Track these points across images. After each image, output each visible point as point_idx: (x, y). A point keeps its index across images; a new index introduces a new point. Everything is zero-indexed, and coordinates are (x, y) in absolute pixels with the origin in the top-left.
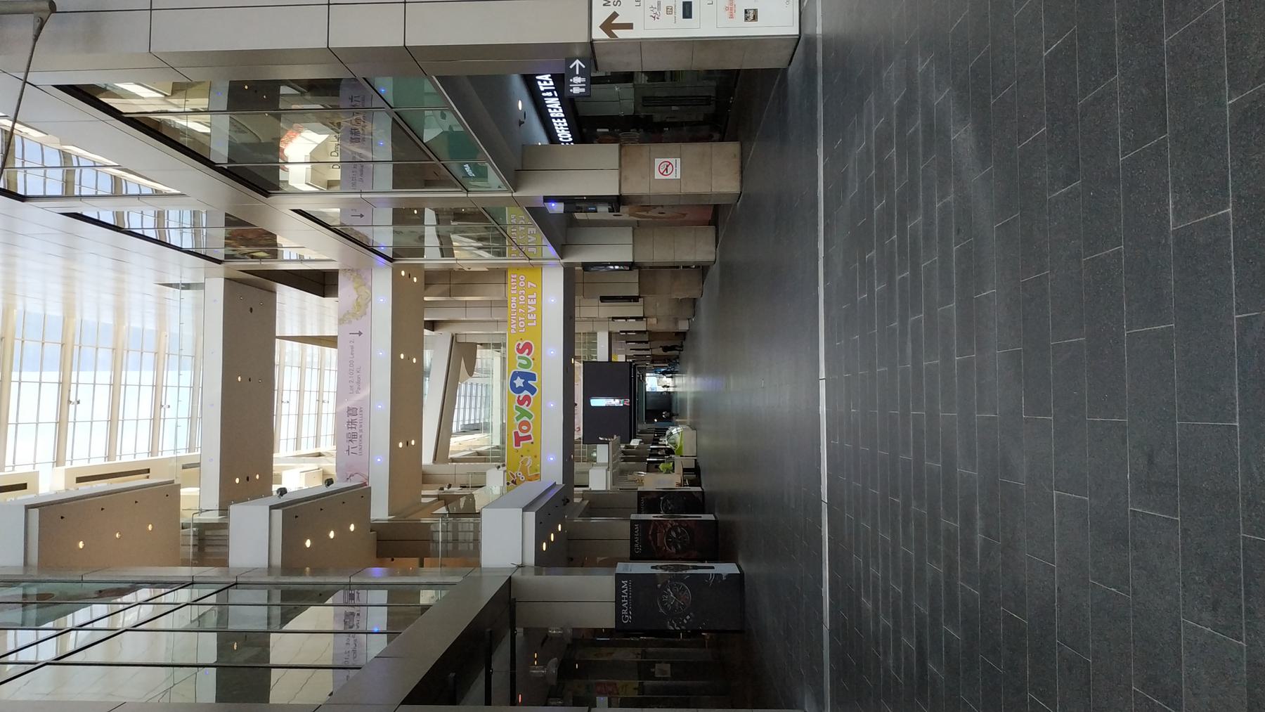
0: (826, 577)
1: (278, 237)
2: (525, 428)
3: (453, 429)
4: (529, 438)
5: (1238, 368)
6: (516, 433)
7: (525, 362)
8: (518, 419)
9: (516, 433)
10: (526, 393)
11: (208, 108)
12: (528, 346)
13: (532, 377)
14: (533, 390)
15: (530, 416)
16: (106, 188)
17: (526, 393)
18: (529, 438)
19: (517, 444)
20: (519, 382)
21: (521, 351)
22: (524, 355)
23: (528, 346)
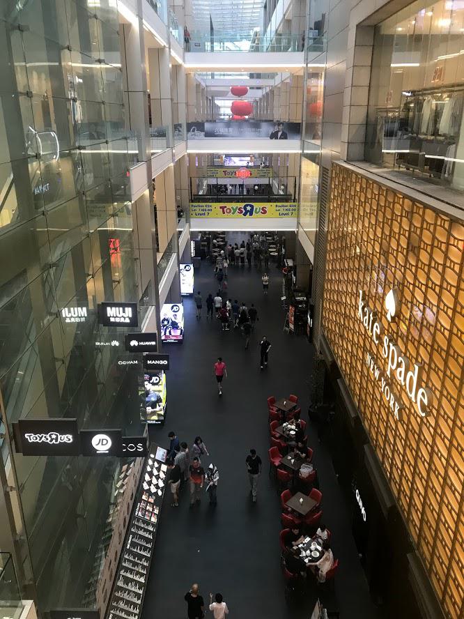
8: (232, 208)
13: (251, 214)
14: (245, 215)
18: (224, 213)
19: (221, 208)
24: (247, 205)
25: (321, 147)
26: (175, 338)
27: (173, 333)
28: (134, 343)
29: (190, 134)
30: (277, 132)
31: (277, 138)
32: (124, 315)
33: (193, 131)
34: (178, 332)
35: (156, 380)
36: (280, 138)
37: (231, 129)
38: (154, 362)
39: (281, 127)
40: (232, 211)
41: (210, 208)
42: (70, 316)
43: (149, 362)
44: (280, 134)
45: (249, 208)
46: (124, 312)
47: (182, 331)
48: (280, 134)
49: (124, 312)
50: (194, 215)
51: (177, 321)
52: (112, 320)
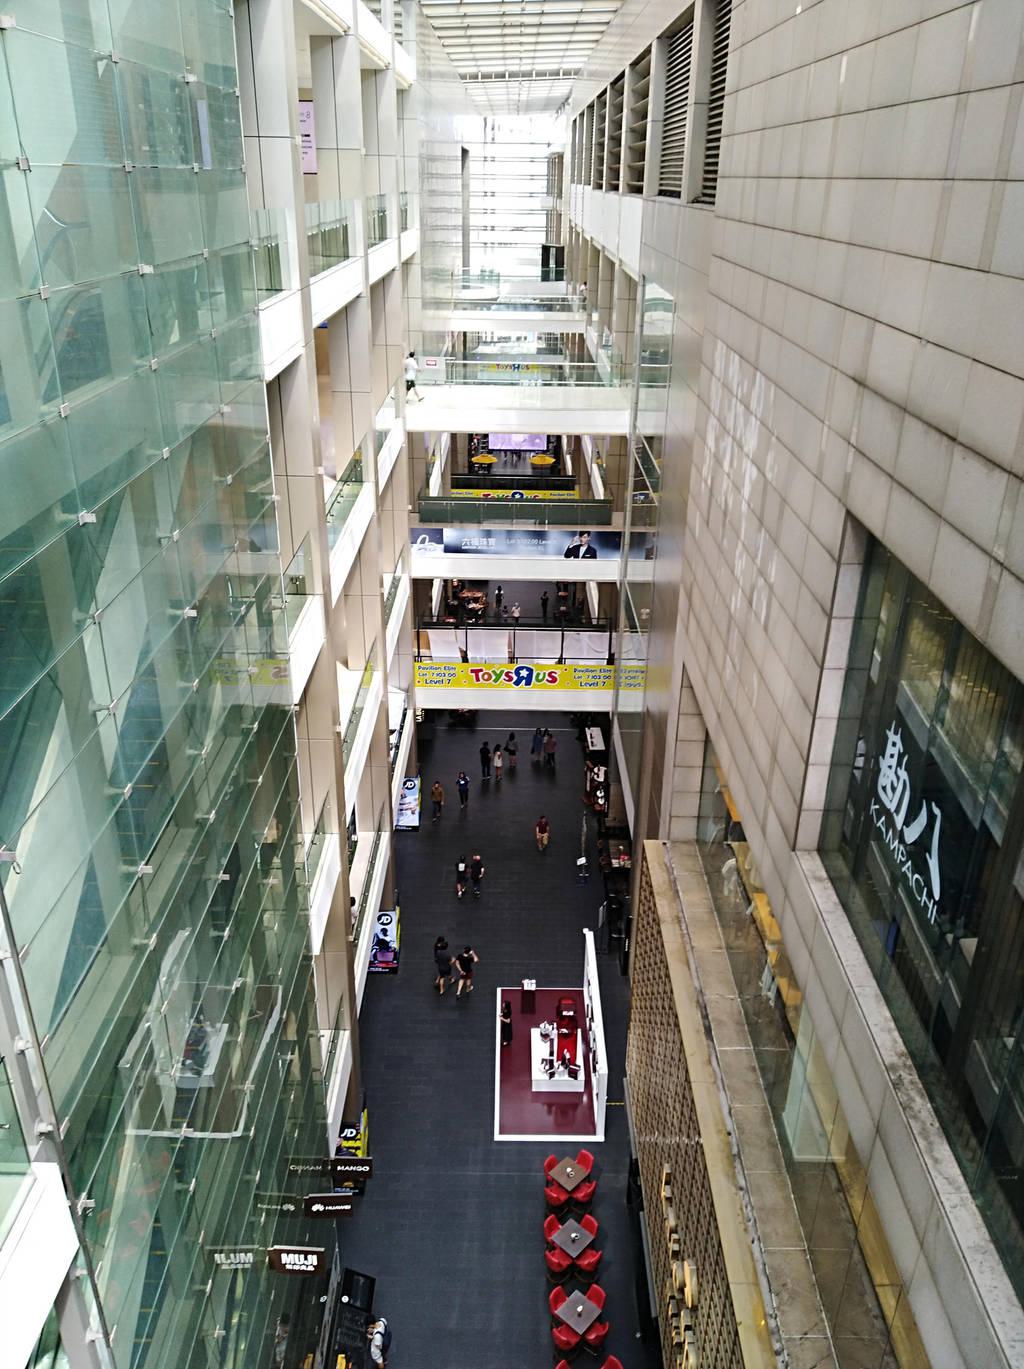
0: (594, 609)
1: (271, 572)
2: (486, 677)
3: (268, 945)
4: (478, 680)
5: (246, 1231)
6: (481, 670)
7: (541, 677)
8: (494, 672)
9: (481, 670)
10: (515, 678)
11: (839, 109)
12: (554, 680)
13: (528, 683)
14: (517, 683)
15: (495, 681)
16: (309, 1257)
17: (515, 678)
18: (478, 680)
19: (472, 671)
20: (524, 673)
21: (550, 675)
22: (547, 677)
23: (554, 680)
24: (516, 493)
25: (721, 1083)
26: (384, 965)
27: (380, 959)
28: (316, 1207)
29: (416, 546)
30: (577, 548)
31: (577, 556)
32: (306, 1262)
33: (423, 542)
34: (391, 956)
35: (352, 1133)
36: (583, 557)
37: (492, 541)
38: (347, 1168)
39: (585, 538)
40: (494, 677)
41: (452, 672)
42: (229, 1261)
43: (339, 1168)
44: (583, 550)
45: (524, 673)
46: (306, 1259)
47: (396, 954)
48: (583, 550)
49: (306, 1259)
50: (423, 682)
51: (387, 939)
52: (288, 1267)
